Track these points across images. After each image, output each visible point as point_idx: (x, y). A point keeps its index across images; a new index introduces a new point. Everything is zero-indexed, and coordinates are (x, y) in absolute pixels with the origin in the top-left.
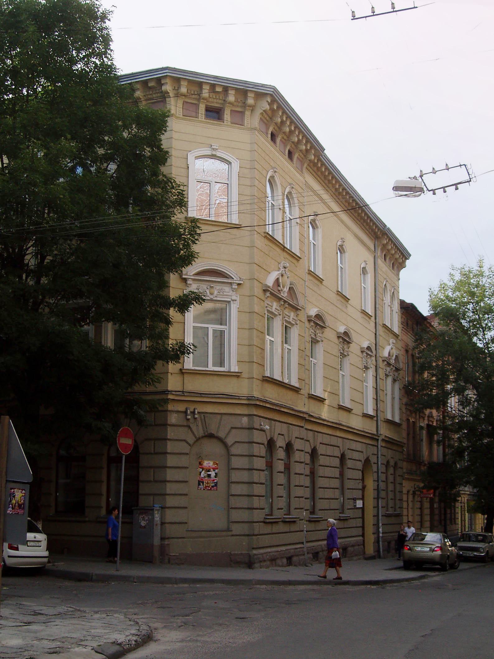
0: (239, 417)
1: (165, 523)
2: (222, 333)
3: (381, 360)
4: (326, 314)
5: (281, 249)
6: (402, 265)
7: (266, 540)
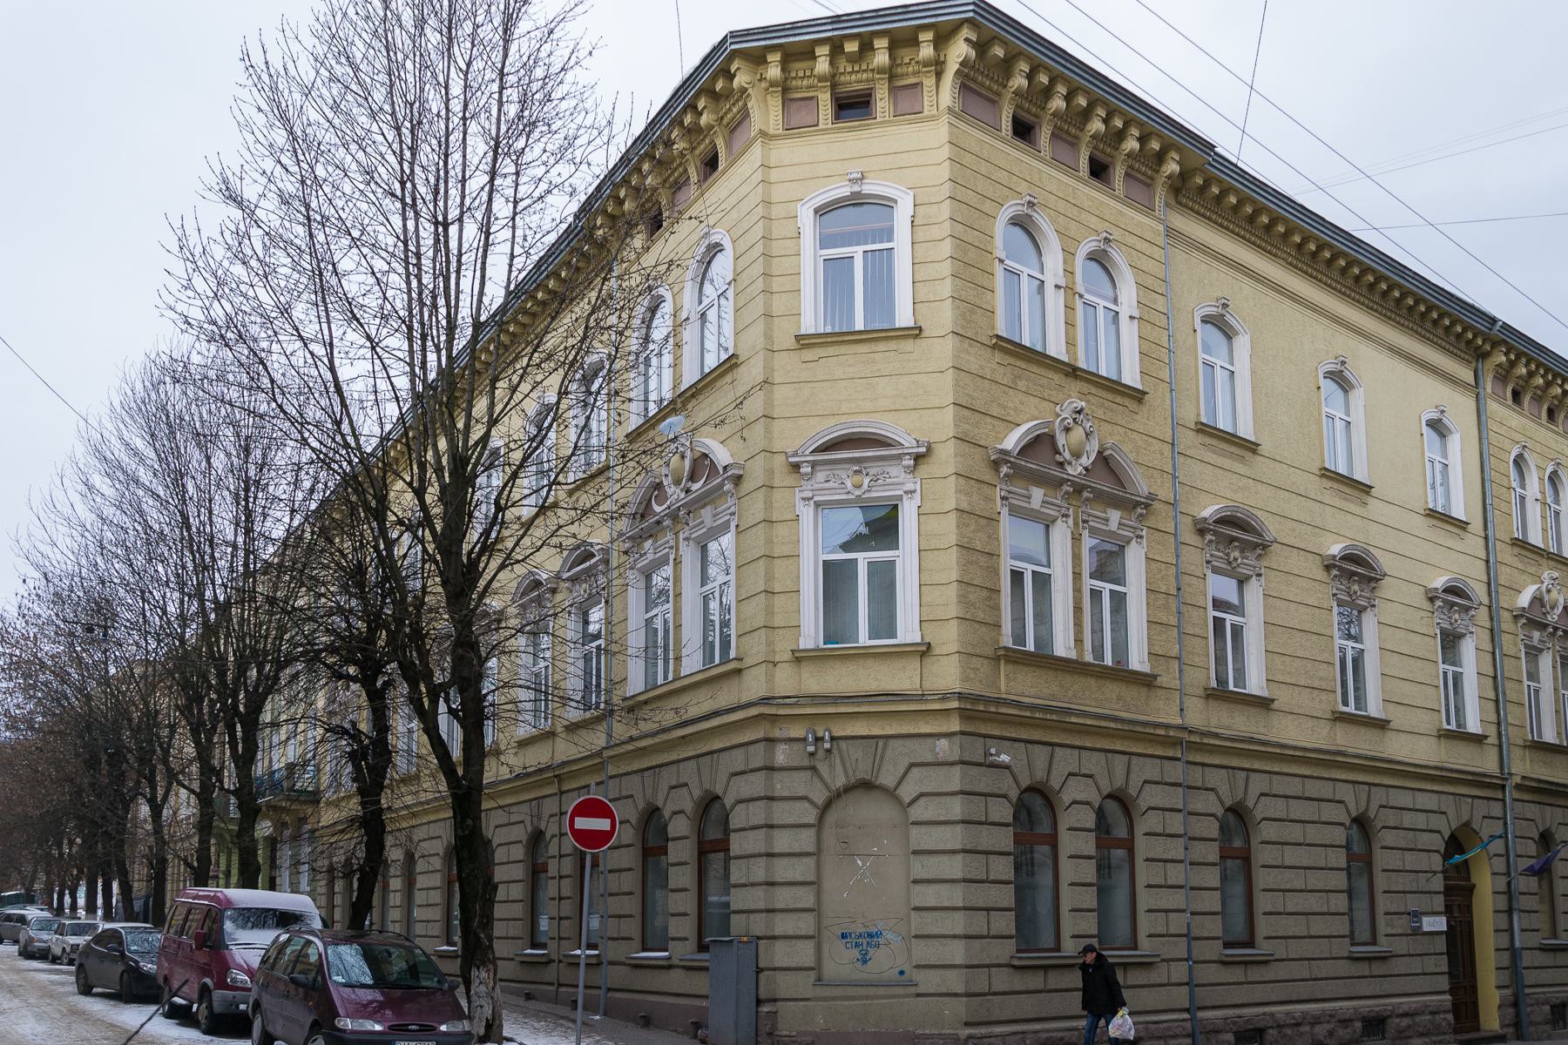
0: (930, 741)
1: (762, 970)
3: (1506, 616)
4: (1259, 513)
7: (1218, 996)
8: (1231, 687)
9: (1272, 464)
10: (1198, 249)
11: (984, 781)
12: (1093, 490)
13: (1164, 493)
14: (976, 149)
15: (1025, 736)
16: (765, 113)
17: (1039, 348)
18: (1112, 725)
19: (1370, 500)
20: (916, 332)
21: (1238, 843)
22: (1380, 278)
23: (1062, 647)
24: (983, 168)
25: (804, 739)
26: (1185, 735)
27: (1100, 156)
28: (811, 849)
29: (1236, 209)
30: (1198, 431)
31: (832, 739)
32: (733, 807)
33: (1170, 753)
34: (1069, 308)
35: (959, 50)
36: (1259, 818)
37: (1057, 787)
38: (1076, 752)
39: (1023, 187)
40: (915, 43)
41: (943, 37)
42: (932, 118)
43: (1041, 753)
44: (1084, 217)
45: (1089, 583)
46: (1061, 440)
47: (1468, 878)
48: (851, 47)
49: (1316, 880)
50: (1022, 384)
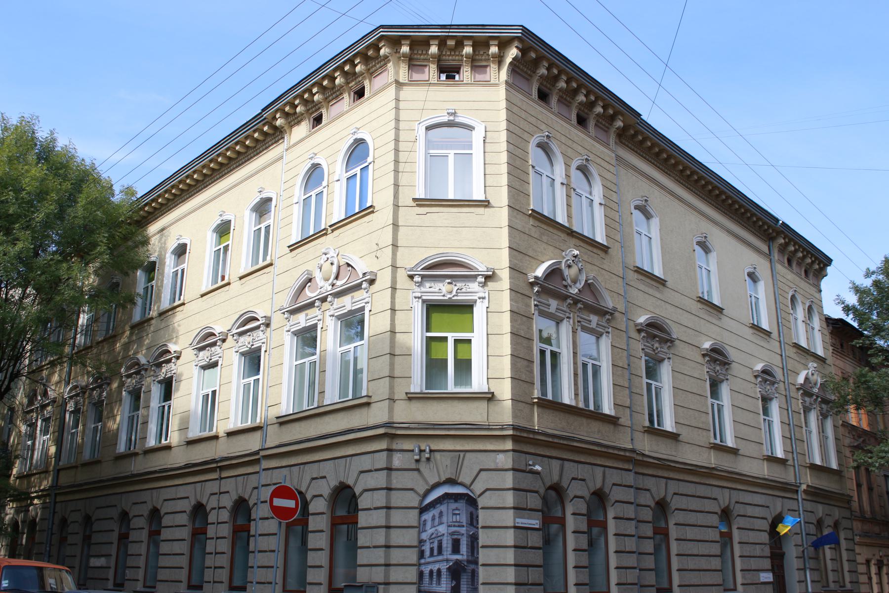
0: (493, 454)
2: (428, 330)
4: (668, 321)
5: (568, 234)
8: (656, 426)
9: (674, 293)
10: (632, 168)
11: (527, 482)
12: (584, 303)
13: (621, 307)
14: (519, 104)
15: (548, 454)
17: (591, 237)
18: (596, 448)
19: (722, 317)
22: (722, 192)
23: (567, 399)
24: (523, 115)
25: (413, 451)
26: (634, 455)
27: (582, 113)
28: (416, 524)
29: (650, 148)
30: (635, 271)
31: (431, 451)
32: (361, 494)
33: (626, 467)
34: (568, 196)
35: (513, 52)
36: (673, 508)
37: (566, 487)
38: (576, 464)
39: (543, 127)
40: (488, 46)
41: (504, 44)
42: (496, 85)
43: (556, 464)
44: (575, 146)
46: (566, 272)
47: (781, 548)
48: (451, 43)
49: (703, 549)
50: (545, 238)
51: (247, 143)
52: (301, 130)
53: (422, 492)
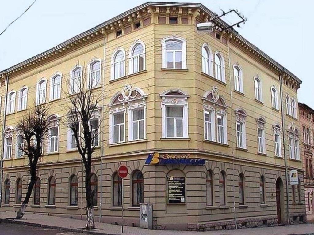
6: (298, 87)
12: (219, 105)
16: (153, 19)
20: (186, 71)
21: (209, 179)
45: (218, 125)
51: (88, 38)
52: (112, 36)
53: (167, 173)
